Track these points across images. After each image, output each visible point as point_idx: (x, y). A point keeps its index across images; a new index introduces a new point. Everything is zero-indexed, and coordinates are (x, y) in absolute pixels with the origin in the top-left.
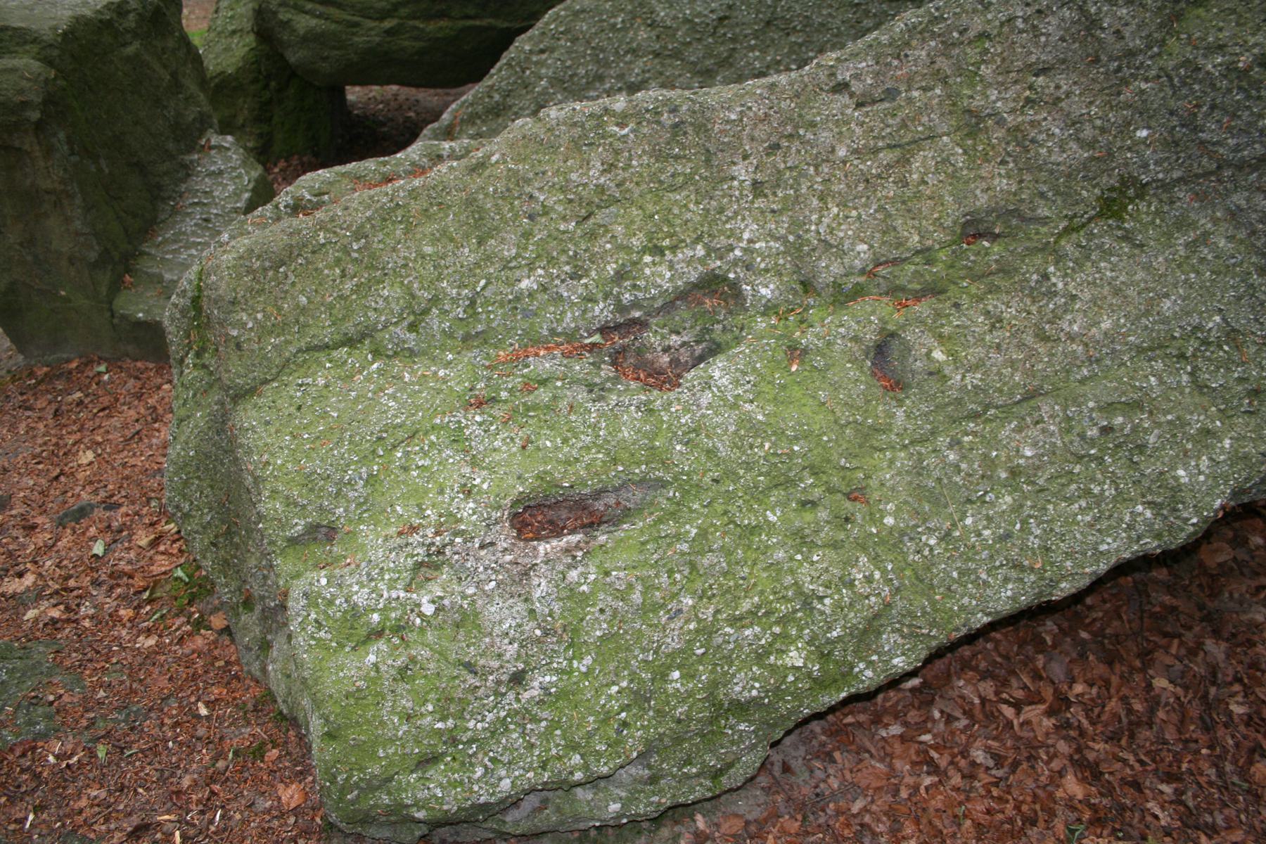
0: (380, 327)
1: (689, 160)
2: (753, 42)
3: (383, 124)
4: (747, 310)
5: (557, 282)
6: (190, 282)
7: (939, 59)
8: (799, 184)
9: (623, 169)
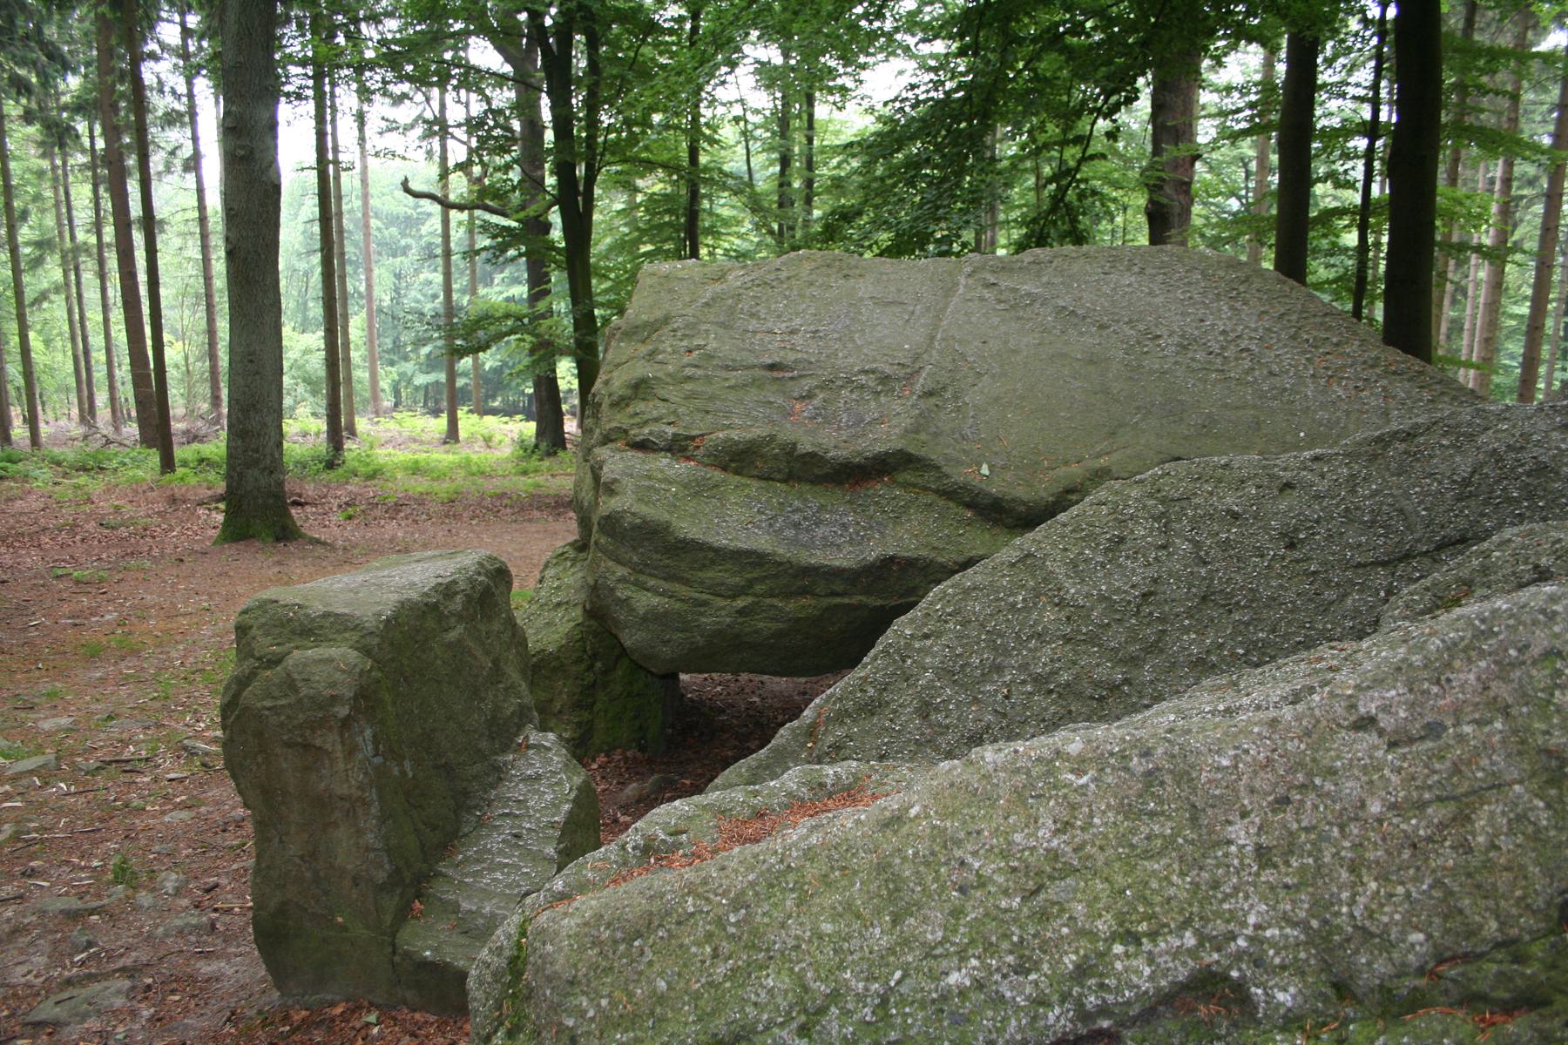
0: (760, 1027)
1: (1169, 818)
2: (1187, 622)
3: (722, 711)
4: (1258, 1022)
5: (997, 977)
6: (509, 937)
7: (1493, 684)
8: (1320, 851)
9: (1083, 829)
